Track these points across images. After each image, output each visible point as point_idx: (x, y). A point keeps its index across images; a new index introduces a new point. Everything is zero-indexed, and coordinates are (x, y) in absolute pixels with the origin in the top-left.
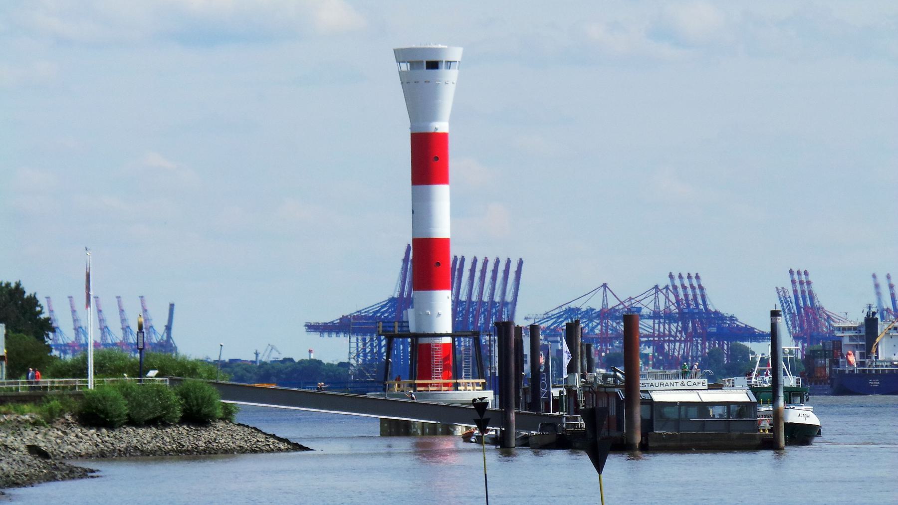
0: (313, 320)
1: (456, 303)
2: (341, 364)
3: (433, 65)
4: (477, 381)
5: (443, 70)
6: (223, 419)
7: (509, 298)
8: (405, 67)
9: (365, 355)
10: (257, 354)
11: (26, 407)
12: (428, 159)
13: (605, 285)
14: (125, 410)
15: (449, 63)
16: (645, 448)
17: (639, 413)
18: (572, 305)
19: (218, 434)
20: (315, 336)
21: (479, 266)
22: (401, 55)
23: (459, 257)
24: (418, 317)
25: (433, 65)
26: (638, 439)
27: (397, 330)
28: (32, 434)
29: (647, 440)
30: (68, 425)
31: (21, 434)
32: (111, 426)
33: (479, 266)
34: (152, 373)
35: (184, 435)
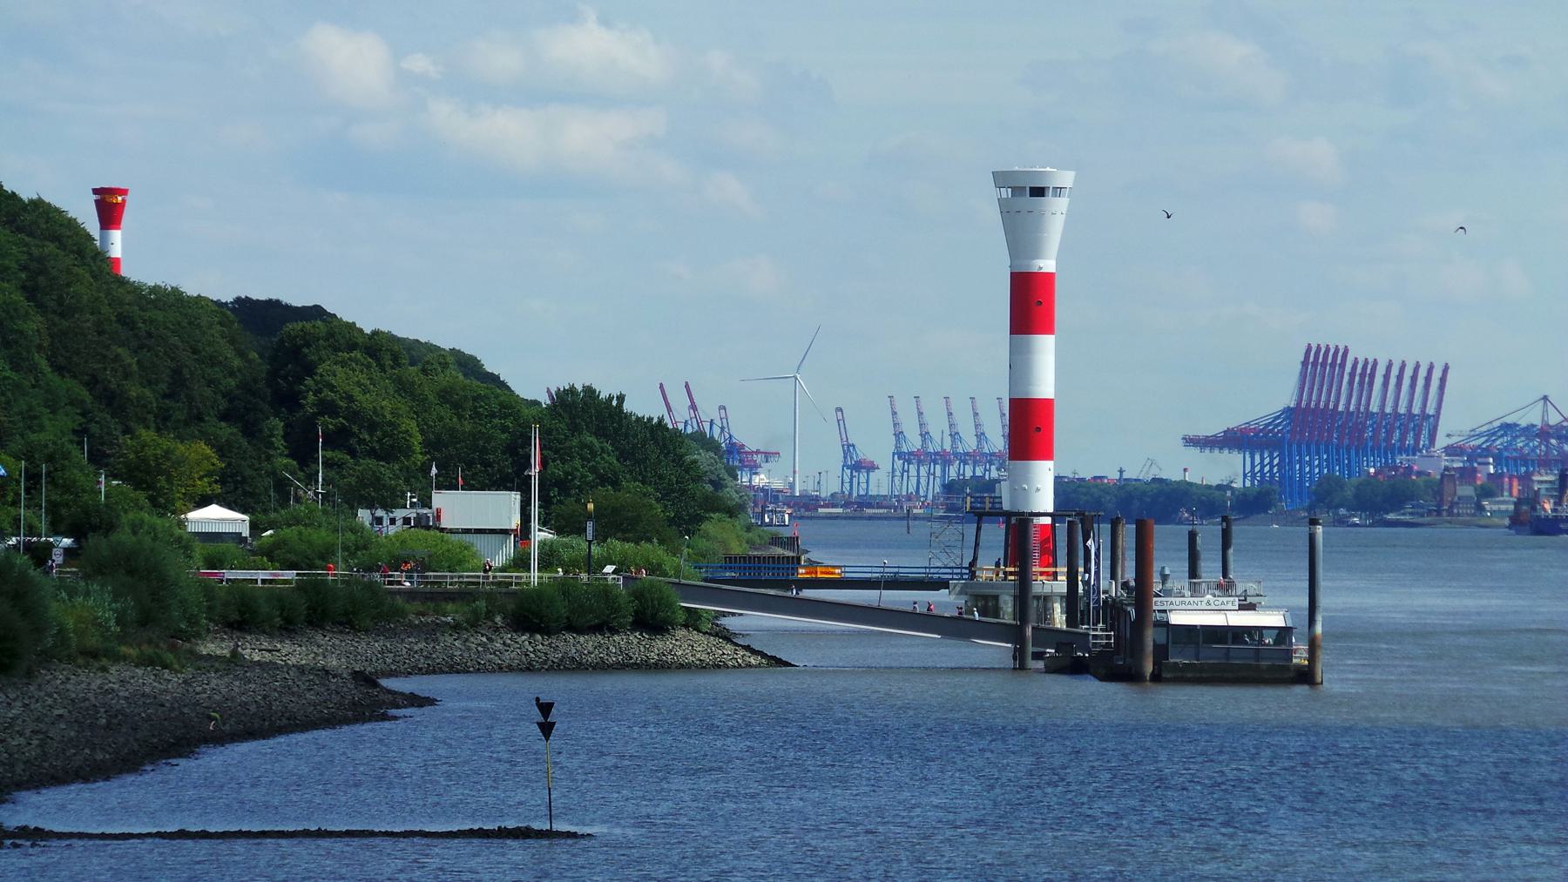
0: (1191, 433)
1: (1058, 480)
2: (1219, 487)
3: (1039, 192)
4: (1506, 486)
5: (1049, 198)
6: (686, 626)
7: (1430, 410)
8: (1006, 193)
9: (1254, 476)
10: (1121, 472)
11: (450, 607)
12: (1030, 304)
13: (1545, 398)
14: (564, 612)
15: (1058, 191)
16: (1157, 678)
17: (1150, 637)
18: (1509, 420)
19: (682, 644)
20: (1194, 451)
21: (1395, 372)
22: (1001, 179)
23: (1371, 361)
24: (1013, 491)
25: (1039, 192)
26: (1149, 668)
27: (988, 506)
28: (449, 640)
29: (1160, 670)
30: (497, 629)
31: (436, 640)
32: (547, 632)
33: (1422, 373)
34: (609, 569)
35: (633, 643)
